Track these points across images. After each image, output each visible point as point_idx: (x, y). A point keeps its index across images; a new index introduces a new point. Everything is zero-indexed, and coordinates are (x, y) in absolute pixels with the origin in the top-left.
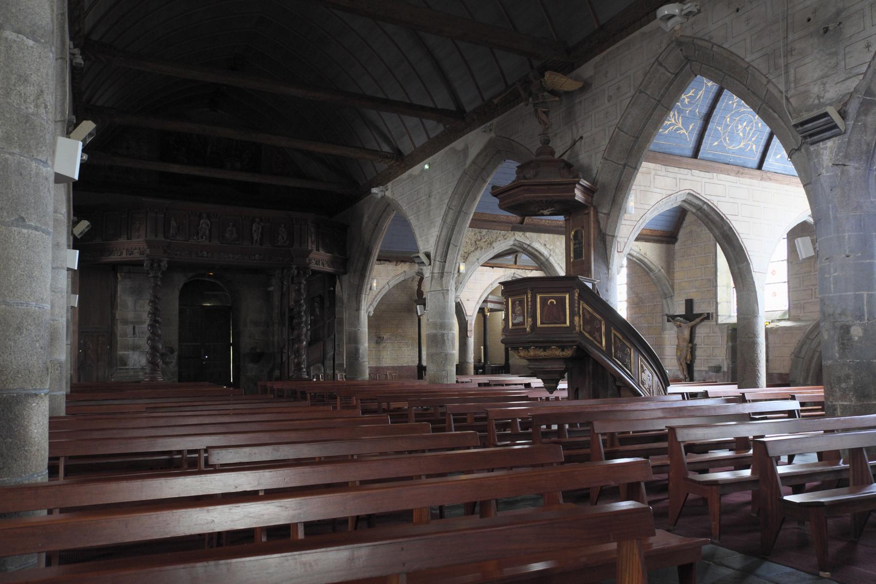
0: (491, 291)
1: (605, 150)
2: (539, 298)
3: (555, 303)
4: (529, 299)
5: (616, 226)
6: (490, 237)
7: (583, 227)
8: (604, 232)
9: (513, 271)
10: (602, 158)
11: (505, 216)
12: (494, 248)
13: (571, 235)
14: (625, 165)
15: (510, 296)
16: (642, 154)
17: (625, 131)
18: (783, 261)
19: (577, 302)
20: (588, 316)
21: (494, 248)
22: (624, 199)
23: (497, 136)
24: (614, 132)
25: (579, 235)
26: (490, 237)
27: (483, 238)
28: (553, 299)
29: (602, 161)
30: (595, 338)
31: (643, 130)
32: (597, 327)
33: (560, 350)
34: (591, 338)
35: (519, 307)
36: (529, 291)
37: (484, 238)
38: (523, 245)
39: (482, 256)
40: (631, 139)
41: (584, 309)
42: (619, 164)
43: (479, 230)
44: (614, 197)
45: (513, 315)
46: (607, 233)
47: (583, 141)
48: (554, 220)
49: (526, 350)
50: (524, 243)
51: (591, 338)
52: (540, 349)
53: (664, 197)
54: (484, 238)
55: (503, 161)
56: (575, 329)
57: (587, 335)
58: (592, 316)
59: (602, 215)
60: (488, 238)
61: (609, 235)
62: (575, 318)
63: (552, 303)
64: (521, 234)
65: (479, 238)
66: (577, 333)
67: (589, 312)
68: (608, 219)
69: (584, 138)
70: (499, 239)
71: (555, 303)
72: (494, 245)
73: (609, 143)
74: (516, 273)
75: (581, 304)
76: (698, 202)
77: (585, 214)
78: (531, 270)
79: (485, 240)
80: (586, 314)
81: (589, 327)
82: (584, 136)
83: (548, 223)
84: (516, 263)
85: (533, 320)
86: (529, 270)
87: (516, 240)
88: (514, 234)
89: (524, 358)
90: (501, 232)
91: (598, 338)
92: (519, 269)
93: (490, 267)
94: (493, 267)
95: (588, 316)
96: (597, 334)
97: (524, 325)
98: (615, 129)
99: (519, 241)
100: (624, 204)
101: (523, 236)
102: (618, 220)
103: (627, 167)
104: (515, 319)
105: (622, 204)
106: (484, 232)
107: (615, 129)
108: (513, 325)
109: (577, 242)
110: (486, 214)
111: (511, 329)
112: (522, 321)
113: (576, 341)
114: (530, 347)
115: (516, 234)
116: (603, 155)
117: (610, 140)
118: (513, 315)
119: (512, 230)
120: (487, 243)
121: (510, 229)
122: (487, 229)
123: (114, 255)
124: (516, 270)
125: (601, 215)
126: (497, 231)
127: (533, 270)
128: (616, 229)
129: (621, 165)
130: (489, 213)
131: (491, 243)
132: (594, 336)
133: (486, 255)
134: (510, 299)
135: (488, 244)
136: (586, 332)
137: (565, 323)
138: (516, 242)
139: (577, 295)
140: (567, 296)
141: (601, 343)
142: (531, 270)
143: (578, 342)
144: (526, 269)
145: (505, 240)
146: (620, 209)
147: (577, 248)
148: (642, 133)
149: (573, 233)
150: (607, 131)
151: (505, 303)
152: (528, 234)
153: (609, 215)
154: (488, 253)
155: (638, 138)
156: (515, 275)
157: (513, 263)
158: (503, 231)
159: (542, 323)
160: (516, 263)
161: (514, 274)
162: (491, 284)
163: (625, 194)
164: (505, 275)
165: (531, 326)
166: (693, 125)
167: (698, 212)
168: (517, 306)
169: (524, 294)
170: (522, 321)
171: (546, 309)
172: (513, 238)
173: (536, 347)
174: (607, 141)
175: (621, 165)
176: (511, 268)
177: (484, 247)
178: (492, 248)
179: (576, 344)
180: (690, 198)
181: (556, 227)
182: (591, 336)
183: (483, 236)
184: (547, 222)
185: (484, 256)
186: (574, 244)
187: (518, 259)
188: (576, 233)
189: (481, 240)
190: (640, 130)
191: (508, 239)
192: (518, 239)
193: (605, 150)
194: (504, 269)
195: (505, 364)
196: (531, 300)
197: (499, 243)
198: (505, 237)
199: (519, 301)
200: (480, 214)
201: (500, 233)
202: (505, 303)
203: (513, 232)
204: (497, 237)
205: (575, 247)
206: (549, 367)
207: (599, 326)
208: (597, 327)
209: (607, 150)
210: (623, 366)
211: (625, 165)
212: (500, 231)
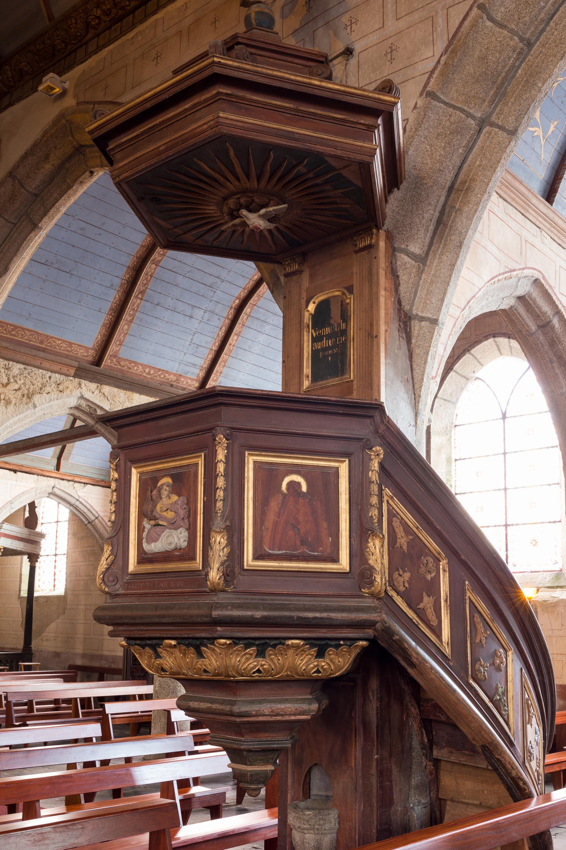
0: (8, 514)
1: (432, 72)
2: (251, 466)
3: (304, 488)
4: (221, 468)
5: (445, 294)
6: (28, 382)
7: (350, 289)
8: (407, 308)
9: (52, 482)
10: (421, 95)
11: (64, 341)
12: (35, 406)
13: (307, 314)
14: (482, 123)
15: (135, 461)
16: (540, 91)
17: (498, 17)
18: (549, 485)
19: (375, 488)
20: (403, 541)
21: (35, 406)
22: (471, 219)
23: (78, 104)
24: (464, 19)
25: (335, 312)
26: (28, 382)
27: (12, 380)
28: (298, 473)
29: (420, 103)
30: (421, 614)
31: (548, 24)
32: (429, 577)
33: (314, 651)
34: (411, 614)
35: (175, 498)
36: (220, 438)
37: (16, 381)
38: (95, 410)
39: (8, 419)
40: (512, 43)
41: (392, 514)
42: (469, 115)
43: (6, 362)
44: (442, 212)
45: (147, 525)
46: (414, 312)
47: (353, 61)
48: (160, 370)
49: (192, 649)
50: (99, 406)
51: (411, 614)
52: (247, 646)
53: (501, 272)
54: (16, 381)
55: (88, 173)
56: (372, 583)
57: (399, 601)
58: (415, 542)
59: (406, 259)
60: (24, 384)
61: (422, 319)
62: (371, 544)
63: (293, 485)
64: (93, 386)
65: (5, 381)
66: (373, 595)
67: (407, 530)
68: (420, 272)
69: (355, 53)
70: (48, 389)
71: (304, 488)
72: (36, 399)
73: (446, 50)
74: (57, 486)
75: (385, 498)
76: (546, 308)
77: (356, 252)
78: (84, 483)
79: (16, 387)
80: (400, 532)
81: (407, 576)
82: (358, 47)
83: (149, 373)
84: (58, 468)
85: (230, 542)
86: (80, 482)
87: (82, 397)
88: (80, 384)
89: (390, 760)
90: (53, 375)
91: (431, 614)
92: (63, 480)
93: (10, 470)
94: (15, 471)
95: (403, 541)
96: (427, 602)
97: (193, 558)
98: (471, 9)
99: (88, 401)
100: (470, 232)
101: (97, 392)
102: (450, 276)
103: (487, 129)
104: (152, 539)
105: (467, 232)
106: (16, 368)
107: (471, 9)
108: (143, 558)
109: (327, 330)
110: (24, 329)
111: (134, 575)
112: (184, 544)
113: (371, 624)
114: (212, 640)
115: (83, 385)
116: (427, 84)
117: (450, 42)
118: (147, 525)
119: (75, 376)
120: (19, 393)
121: (72, 371)
122: (24, 364)
123: (169, 658)
124: (57, 481)
125: (403, 259)
126: (44, 372)
127: (87, 484)
128: (443, 300)
129: (473, 118)
130: (31, 328)
131: (29, 397)
132: (421, 606)
133: (16, 419)
134: (134, 471)
135: (23, 396)
136: (398, 593)
137: (335, 559)
138: (83, 404)
139: (375, 465)
140: (344, 468)
141: (437, 632)
142: (84, 483)
143: (378, 626)
144: (75, 482)
145: (60, 394)
146: (460, 247)
147: (324, 349)
148: (543, 30)
149: (312, 307)
150: (440, 21)
151: (113, 485)
152: (107, 389)
153: (424, 264)
154: (22, 416)
155: (530, 45)
156: (55, 490)
157: (52, 467)
158: (57, 375)
159: (257, 556)
160: (58, 468)
161: (53, 488)
162: (11, 502)
163: (478, 204)
164: (37, 489)
165: (222, 564)
166: (556, 123)
167: (539, 332)
168: (165, 493)
169: (196, 450)
170: (184, 544)
171: (274, 505)
172: (77, 393)
173: (236, 640)
174: (441, 46)
175: (473, 118)
176: (48, 476)
177: (13, 402)
178: (30, 405)
179: (370, 633)
180: (536, 295)
181: (162, 383)
182: (410, 606)
183: (14, 377)
184: (147, 370)
185: (11, 421)
186: (315, 340)
187: (62, 461)
188: (323, 308)
189: (7, 384)
190: (542, 20)
191: (67, 392)
192: (88, 395)
193: (432, 72)
194: (35, 476)
195: (23, 650)
196: (225, 470)
197: (47, 396)
198: (61, 387)
199: (172, 476)
200: (10, 328)
201: (50, 377)
202: (113, 485)
203: (77, 380)
204: (44, 385)
205: (319, 346)
206: (266, 708)
207: (433, 575)
208: (429, 577)
209: (437, 72)
210: (490, 705)
211: (482, 123)
212: (50, 374)
